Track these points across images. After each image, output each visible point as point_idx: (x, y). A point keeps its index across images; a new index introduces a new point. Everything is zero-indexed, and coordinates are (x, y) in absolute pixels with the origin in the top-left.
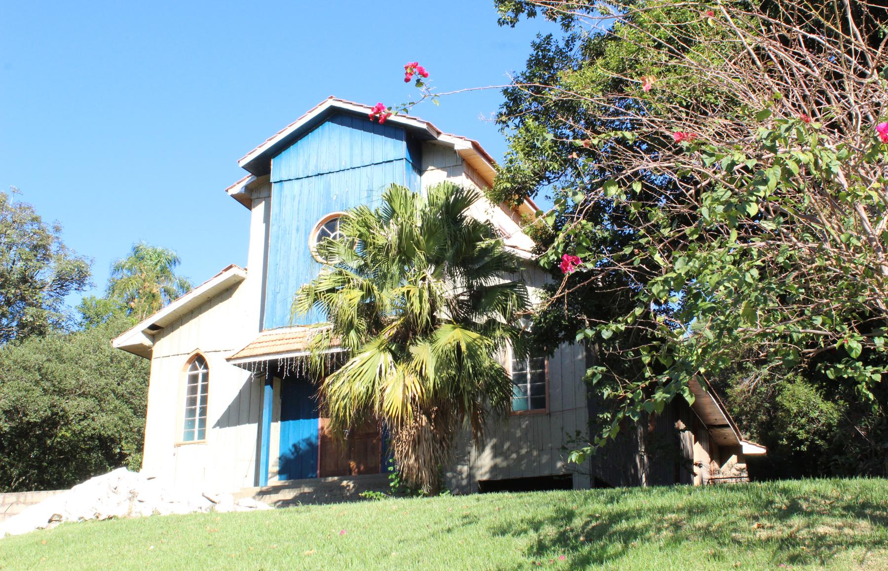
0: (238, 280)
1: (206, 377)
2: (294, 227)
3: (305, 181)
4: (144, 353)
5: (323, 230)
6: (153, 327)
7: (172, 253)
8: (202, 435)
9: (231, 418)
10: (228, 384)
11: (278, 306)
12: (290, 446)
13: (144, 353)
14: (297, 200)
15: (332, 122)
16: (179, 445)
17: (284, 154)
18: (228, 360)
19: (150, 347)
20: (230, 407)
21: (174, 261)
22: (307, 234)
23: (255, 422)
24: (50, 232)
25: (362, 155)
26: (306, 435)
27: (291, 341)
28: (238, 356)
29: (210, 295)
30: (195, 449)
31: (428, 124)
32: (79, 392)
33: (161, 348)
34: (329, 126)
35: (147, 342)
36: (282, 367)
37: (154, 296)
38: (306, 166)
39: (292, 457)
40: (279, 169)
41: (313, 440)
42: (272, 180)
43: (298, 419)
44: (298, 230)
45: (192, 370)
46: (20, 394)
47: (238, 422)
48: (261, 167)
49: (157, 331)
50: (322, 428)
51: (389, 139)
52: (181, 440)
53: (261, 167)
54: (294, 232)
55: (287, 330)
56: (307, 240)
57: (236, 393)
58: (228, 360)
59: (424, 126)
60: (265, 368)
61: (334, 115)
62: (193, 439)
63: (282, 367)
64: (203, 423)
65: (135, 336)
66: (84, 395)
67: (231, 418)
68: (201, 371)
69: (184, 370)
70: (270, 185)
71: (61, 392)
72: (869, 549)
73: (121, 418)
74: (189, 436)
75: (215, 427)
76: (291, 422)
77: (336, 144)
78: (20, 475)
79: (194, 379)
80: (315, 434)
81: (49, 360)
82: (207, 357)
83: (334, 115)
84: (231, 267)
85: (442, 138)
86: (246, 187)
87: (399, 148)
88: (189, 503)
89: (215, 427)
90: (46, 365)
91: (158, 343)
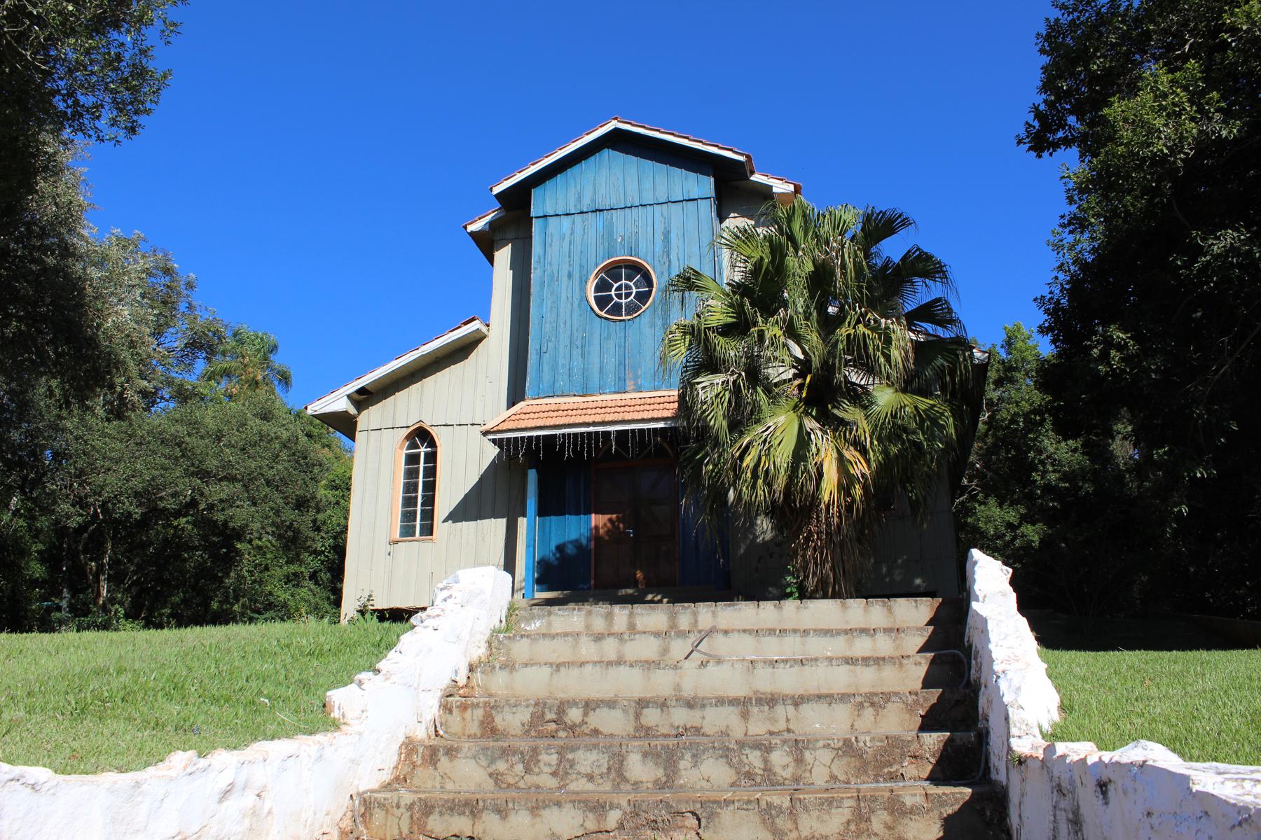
0: (478, 336)
1: (432, 457)
2: (564, 272)
3: (578, 218)
4: (345, 424)
5: (602, 278)
6: (362, 391)
7: (273, 338)
8: (428, 530)
9: (468, 510)
10: (463, 464)
11: (546, 368)
12: (553, 548)
13: (345, 424)
14: (567, 240)
15: (614, 149)
16: (396, 542)
17: (560, 178)
18: (485, 433)
19: (355, 417)
20: (466, 496)
21: (274, 348)
22: (583, 283)
23: (495, 515)
24: (182, 288)
25: (654, 189)
26: (573, 536)
27: (570, 413)
28: (499, 428)
29: (439, 355)
30: (415, 548)
31: (747, 156)
32: (221, 474)
33: (369, 418)
34: (607, 154)
35: (352, 410)
36: (562, 445)
37: (257, 383)
38: (579, 199)
39: (556, 563)
40: (540, 202)
41: (584, 542)
42: (532, 214)
43: (563, 514)
44: (570, 276)
45: (409, 448)
46: (157, 473)
47: (479, 516)
48: (516, 204)
49: (365, 398)
50: (597, 528)
51: (692, 175)
52: (397, 536)
53: (516, 204)
54: (565, 279)
55: (618, 396)
56: (583, 289)
57: (474, 479)
58: (485, 433)
59: (742, 159)
60: (537, 445)
61: (618, 141)
62: (414, 535)
63: (562, 445)
64: (429, 515)
65: (338, 402)
66: (232, 479)
67: (468, 510)
68: (423, 450)
69: (401, 448)
70: (528, 221)
71: (205, 475)
72: (714, 627)
73: (272, 509)
74: (408, 531)
75: (445, 521)
76: (553, 518)
77: (618, 176)
78: (135, 573)
79: (412, 459)
80: (587, 534)
81: (189, 435)
82: (439, 435)
83: (618, 141)
84: (473, 320)
85: (757, 178)
86: (491, 223)
87: (704, 185)
88: (400, 616)
89: (445, 521)
90: (187, 439)
91: (365, 413)
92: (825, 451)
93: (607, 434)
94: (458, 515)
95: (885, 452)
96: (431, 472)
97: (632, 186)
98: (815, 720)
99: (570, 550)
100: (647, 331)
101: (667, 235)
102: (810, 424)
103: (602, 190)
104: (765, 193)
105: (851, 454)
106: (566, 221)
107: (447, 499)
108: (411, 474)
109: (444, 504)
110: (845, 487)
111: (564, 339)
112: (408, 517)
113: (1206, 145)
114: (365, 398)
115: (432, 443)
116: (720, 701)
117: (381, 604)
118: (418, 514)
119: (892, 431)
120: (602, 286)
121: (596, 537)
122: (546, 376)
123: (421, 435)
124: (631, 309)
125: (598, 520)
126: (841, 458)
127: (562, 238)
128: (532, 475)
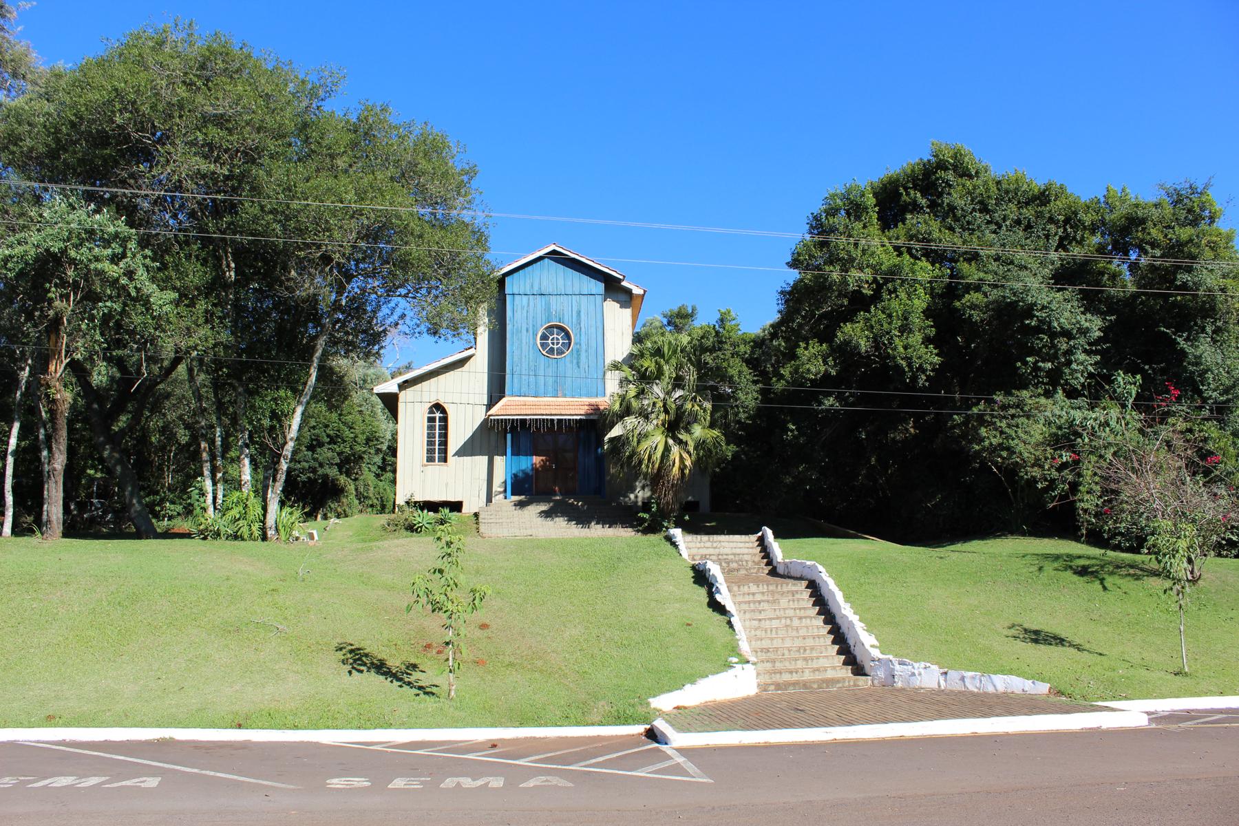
1: (445, 420)
8: (445, 461)
9: (468, 449)
30: (436, 468)
49: (404, 386)
61: (555, 256)
68: (438, 415)
74: (430, 459)
79: (431, 420)
83: (555, 256)
92: (676, 450)
93: (552, 420)
94: (462, 452)
95: (698, 454)
96: (445, 427)
97: (561, 282)
98: (746, 557)
99: (520, 475)
100: (569, 365)
101: (579, 313)
102: (671, 442)
103: (544, 283)
104: (628, 292)
105: (685, 455)
106: (525, 298)
107: (454, 444)
108: (431, 428)
109: (453, 447)
110: (682, 469)
111: (525, 366)
112: (430, 451)
113: (827, 375)
114: (404, 386)
115: (444, 411)
116: (187, 536)
117: (419, 497)
118: (438, 449)
119: (700, 445)
120: (544, 337)
121: (535, 469)
122: (516, 385)
123: (438, 407)
124: (560, 352)
125: (537, 460)
126: (681, 457)
127: (523, 308)
128: (509, 436)
